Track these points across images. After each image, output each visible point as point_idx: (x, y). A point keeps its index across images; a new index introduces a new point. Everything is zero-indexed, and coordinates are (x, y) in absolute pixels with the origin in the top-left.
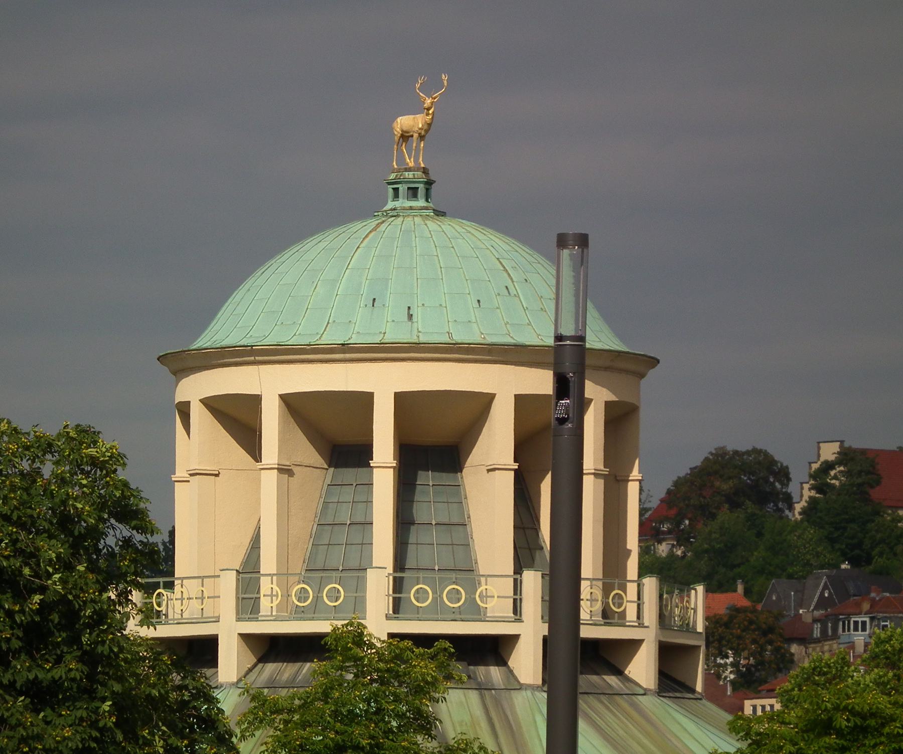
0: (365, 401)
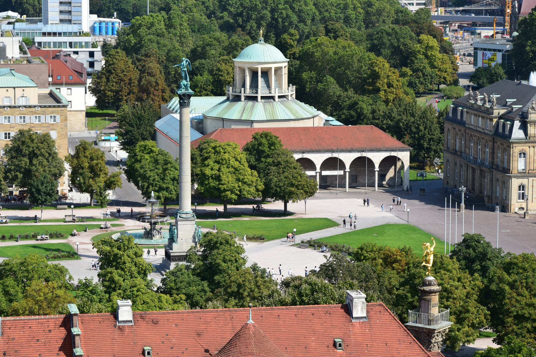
0: (271, 68)
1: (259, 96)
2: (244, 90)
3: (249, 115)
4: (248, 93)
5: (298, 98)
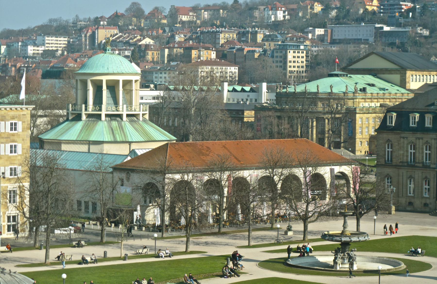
0: (118, 81)
1: (103, 113)
2: (86, 107)
3: (122, 133)
4: (90, 110)
5: (151, 120)
